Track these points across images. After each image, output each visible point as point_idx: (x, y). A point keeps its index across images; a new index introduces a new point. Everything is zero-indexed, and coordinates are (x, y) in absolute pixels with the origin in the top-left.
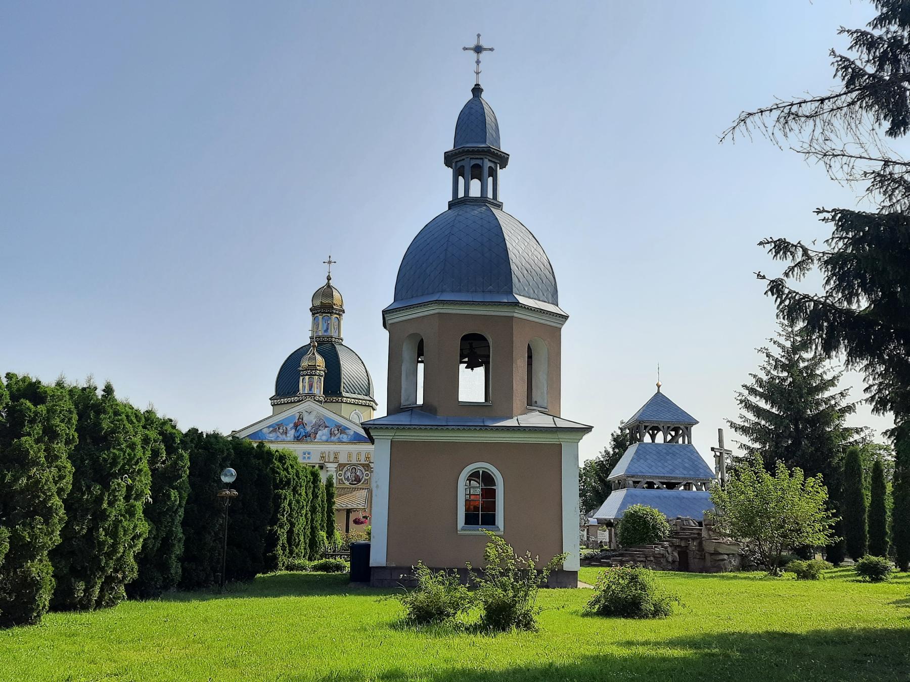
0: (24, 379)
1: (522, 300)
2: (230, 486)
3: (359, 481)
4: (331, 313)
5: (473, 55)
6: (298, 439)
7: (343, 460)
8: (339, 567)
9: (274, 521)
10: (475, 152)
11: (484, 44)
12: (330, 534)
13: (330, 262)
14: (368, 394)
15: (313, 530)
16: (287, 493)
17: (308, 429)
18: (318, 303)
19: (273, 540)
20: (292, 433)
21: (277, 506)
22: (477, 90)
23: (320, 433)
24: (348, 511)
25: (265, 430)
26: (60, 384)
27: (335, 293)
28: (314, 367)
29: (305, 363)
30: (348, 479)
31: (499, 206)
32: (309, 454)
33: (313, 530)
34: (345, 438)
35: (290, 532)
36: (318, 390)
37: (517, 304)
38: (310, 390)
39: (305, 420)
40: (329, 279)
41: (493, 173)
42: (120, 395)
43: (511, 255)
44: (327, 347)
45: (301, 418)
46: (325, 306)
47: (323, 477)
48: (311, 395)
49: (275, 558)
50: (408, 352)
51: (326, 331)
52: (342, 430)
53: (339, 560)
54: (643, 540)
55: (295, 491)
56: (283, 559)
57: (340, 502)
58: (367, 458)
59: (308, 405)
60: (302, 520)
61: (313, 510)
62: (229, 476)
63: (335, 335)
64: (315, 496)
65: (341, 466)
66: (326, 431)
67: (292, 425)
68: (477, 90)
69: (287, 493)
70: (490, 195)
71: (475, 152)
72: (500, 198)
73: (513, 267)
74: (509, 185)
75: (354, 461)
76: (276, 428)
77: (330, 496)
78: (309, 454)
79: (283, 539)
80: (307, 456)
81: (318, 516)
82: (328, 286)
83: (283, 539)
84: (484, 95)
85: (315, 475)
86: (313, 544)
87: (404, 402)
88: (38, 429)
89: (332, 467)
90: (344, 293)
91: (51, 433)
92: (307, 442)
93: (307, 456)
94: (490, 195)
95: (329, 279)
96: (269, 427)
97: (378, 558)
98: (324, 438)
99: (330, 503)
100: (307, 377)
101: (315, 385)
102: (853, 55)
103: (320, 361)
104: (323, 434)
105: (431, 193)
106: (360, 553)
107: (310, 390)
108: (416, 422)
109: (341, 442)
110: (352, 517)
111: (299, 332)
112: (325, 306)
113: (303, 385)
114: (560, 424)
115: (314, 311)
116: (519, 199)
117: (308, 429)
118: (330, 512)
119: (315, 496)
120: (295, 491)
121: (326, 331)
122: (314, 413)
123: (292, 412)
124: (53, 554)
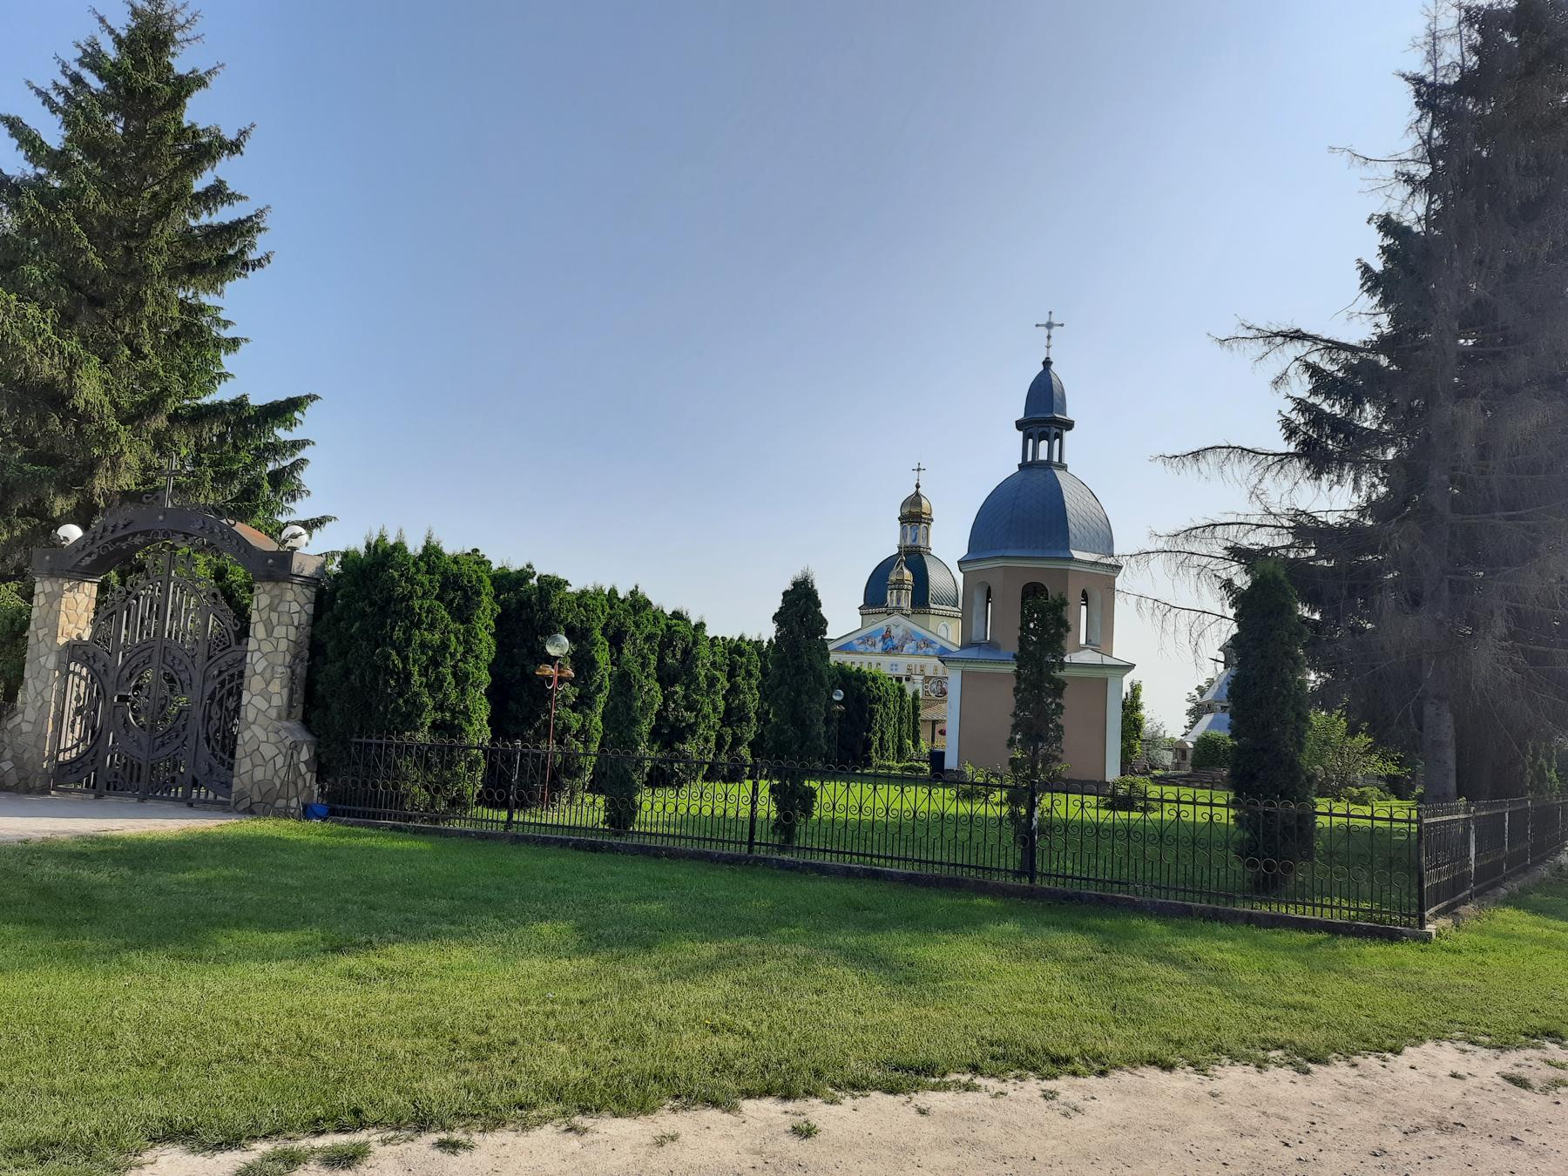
1: (1077, 554)
2: (839, 703)
5: (1044, 331)
6: (886, 651)
7: (929, 673)
8: (921, 769)
9: (869, 729)
10: (1044, 416)
11: (1055, 320)
12: (916, 743)
13: (1049, 325)
15: (900, 739)
16: (879, 707)
17: (896, 642)
18: (906, 511)
19: (868, 745)
20: (880, 645)
21: (872, 717)
22: (1047, 363)
24: (934, 723)
26: (741, 638)
27: (924, 501)
28: (902, 582)
29: (893, 578)
31: (1064, 467)
33: (900, 739)
35: (881, 739)
36: (906, 603)
37: (1072, 559)
41: (1059, 436)
43: (1069, 515)
44: (914, 557)
45: (889, 631)
46: (914, 515)
47: (909, 691)
48: (899, 609)
49: (870, 758)
50: (979, 598)
52: (928, 643)
53: (925, 766)
54: (1213, 763)
55: (885, 705)
56: (876, 761)
57: (925, 714)
59: (896, 618)
60: (891, 730)
61: (900, 721)
62: (838, 696)
63: (922, 543)
64: (902, 709)
65: (927, 679)
68: (1047, 363)
69: (879, 707)
70: (1056, 459)
71: (1044, 416)
72: (1066, 461)
73: (1070, 525)
74: (1074, 447)
76: (865, 640)
77: (916, 708)
79: (876, 744)
81: (905, 727)
82: (917, 494)
83: (876, 744)
84: (1053, 367)
85: (902, 690)
86: (900, 751)
87: (975, 639)
88: (743, 672)
89: (919, 679)
90: (934, 501)
91: (749, 674)
94: (1056, 459)
97: (951, 762)
99: (916, 715)
102: (1293, 416)
103: (908, 574)
104: (909, 647)
105: (1003, 456)
106: (937, 758)
108: (982, 657)
109: (927, 655)
110: (938, 727)
111: (888, 543)
112: (914, 515)
113: (891, 598)
114: (1107, 661)
115: (903, 519)
116: (1083, 459)
117: (896, 642)
118: (916, 723)
119: (902, 709)
120: (885, 705)
123: (882, 623)
124: (750, 745)
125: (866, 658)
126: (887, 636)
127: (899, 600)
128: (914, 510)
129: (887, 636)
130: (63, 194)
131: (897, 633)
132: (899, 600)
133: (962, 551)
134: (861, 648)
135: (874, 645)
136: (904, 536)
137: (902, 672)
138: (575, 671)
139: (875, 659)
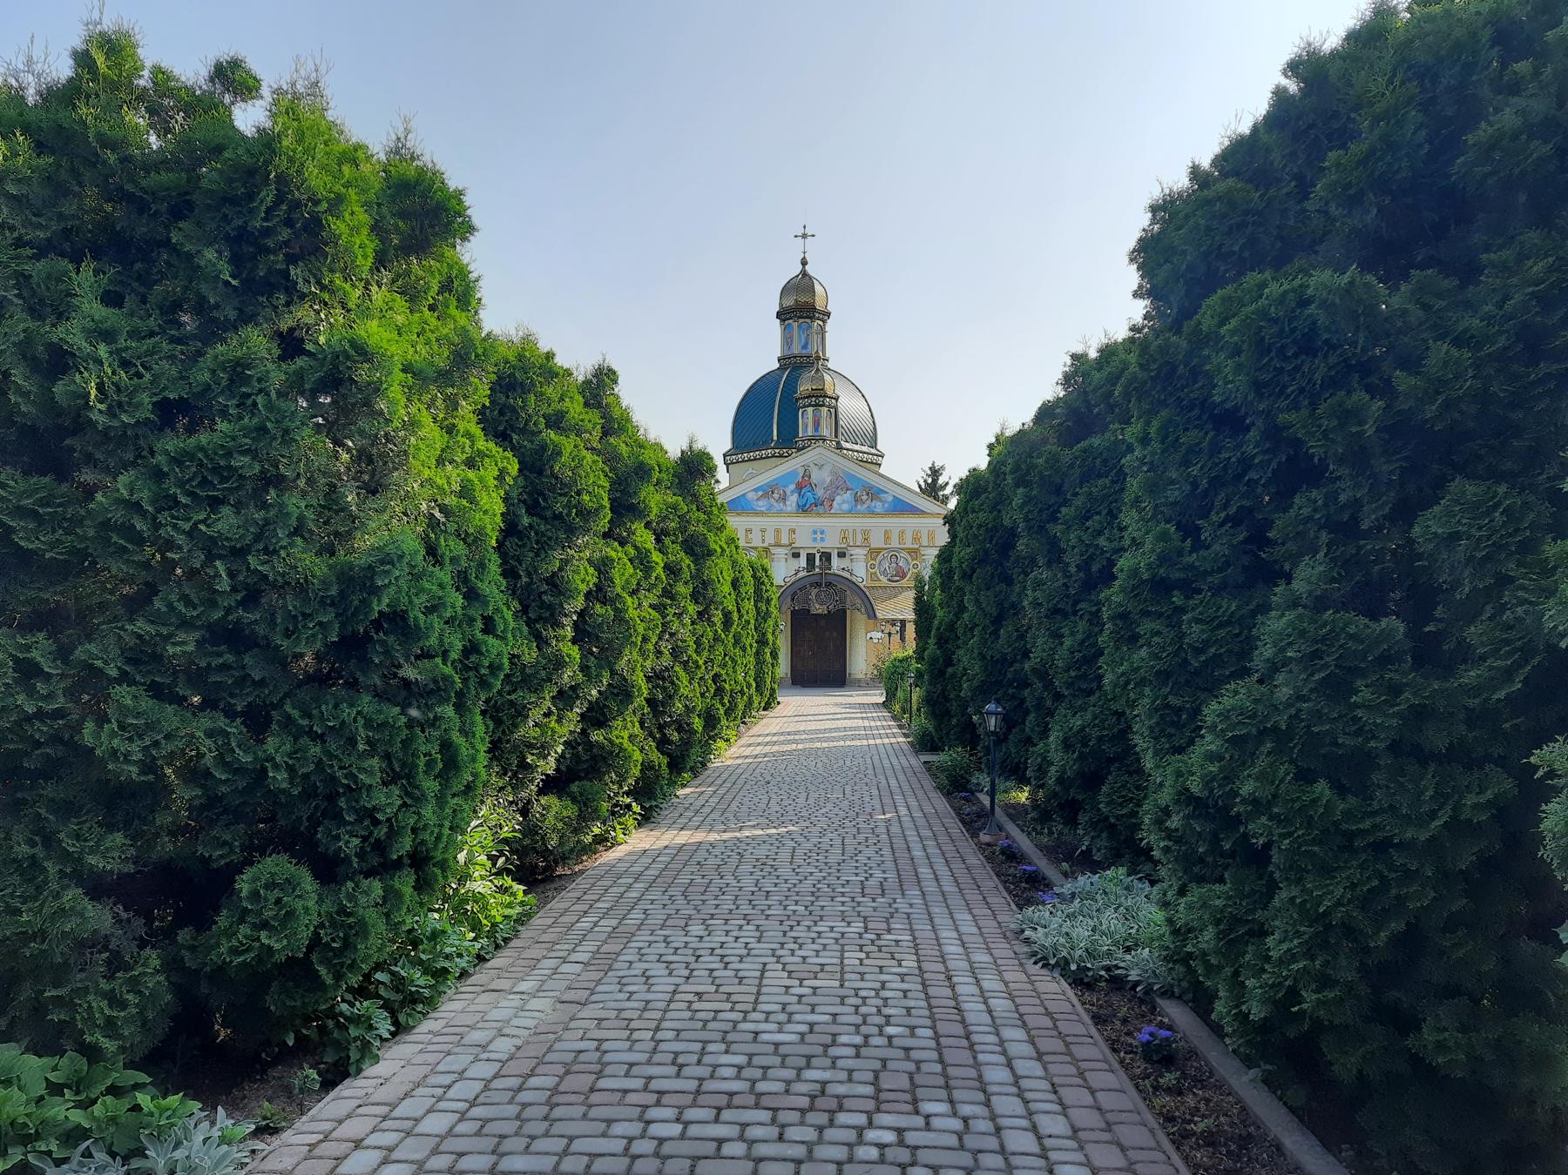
0: (422, 171)
3: (904, 576)
4: (812, 318)
6: (804, 509)
7: (877, 541)
13: (804, 236)
14: (874, 446)
17: (820, 493)
18: (789, 302)
20: (793, 499)
23: (838, 499)
25: (751, 496)
27: (818, 288)
30: (884, 573)
32: (815, 532)
34: (878, 506)
38: (816, 430)
39: (814, 479)
40: (804, 263)
42: (630, 394)
45: (807, 475)
51: (805, 347)
52: (873, 493)
58: (916, 539)
65: (874, 553)
66: (848, 496)
67: (792, 487)
71: (801, 308)
75: (895, 544)
78: (815, 532)
80: (819, 536)
82: (804, 274)
89: (860, 553)
92: (819, 515)
93: (819, 536)
95: (804, 263)
96: (756, 490)
98: (845, 507)
100: (810, 410)
101: (823, 423)
104: (843, 500)
107: (816, 430)
109: (871, 513)
115: (783, 315)
117: (820, 493)
121: (805, 347)
122: (827, 468)
125: (770, 523)
126: (804, 485)
127: (817, 425)
128: (803, 299)
129: (804, 485)
130: (536, 621)
131: (821, 477)
132: (817, 425)
133: (727, 445)
134: (762, 505)
135: (784, 499)
136: (787, 340)
137: (831, 543)
138: (1327, 609)
139: (786, 523)
